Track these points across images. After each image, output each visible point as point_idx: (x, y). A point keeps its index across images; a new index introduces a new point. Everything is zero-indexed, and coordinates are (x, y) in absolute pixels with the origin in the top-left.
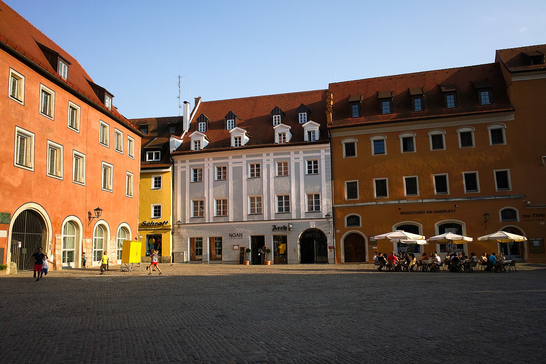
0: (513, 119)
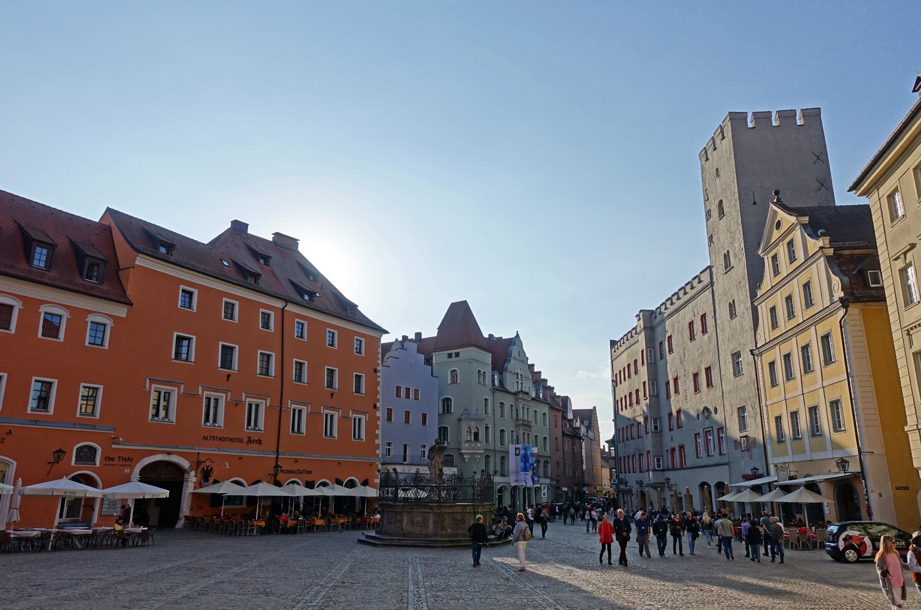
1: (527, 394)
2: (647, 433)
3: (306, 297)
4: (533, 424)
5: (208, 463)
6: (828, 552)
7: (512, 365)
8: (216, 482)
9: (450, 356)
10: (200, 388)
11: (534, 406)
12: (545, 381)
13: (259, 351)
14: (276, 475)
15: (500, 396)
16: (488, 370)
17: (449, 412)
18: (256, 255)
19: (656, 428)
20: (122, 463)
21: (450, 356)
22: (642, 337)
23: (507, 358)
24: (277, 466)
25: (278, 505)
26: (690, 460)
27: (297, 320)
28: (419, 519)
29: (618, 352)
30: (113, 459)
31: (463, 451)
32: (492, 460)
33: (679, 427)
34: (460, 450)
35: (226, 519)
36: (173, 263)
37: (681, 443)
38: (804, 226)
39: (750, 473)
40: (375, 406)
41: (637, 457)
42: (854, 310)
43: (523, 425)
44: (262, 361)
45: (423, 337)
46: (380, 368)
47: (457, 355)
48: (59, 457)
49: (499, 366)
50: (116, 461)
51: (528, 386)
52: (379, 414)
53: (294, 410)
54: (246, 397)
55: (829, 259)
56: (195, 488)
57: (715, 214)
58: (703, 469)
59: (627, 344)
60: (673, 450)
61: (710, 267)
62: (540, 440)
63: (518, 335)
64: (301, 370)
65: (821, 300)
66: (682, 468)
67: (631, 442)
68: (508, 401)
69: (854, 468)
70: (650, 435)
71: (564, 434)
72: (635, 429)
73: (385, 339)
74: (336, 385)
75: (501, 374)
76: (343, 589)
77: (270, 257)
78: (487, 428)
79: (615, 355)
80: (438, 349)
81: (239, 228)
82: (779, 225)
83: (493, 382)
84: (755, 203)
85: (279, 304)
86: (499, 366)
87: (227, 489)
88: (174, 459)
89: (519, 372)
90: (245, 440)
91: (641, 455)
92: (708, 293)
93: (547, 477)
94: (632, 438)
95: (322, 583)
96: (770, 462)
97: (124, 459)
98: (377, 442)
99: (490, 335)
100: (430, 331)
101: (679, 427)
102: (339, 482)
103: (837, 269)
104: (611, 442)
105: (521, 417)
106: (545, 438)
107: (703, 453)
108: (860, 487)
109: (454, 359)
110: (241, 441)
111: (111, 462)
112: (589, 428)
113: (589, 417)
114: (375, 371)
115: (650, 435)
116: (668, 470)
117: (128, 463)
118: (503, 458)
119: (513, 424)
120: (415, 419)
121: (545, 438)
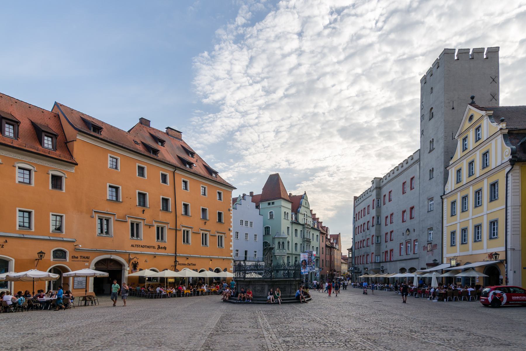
0: (73, 171)
1: (309, 225)
2: (372, 244)
3: (188, 166)
4: (311, 240)
5: (135, 259)
6: (482, 302)
7: (302, 210)
8: (141, 270)
9: (269, 204)
11: (312, 232)
12: (318, 219)
14: (176, 266)
15: (295, 227)
16: (290, 212)
17: (268, 234)
18: (156, 139)
19: (378, 241)
20: (82, 260)
21: (269, 204)
22: (374, 193)
23: (299, 205)
24: (176, 261)
25: (179, 282)
26: (394, 258)
28: (259, 288)
29: (359, 202)
30: (77, 258)
32: (291, 258)
33: (391, 240)
35: (146, 290)
36: (101, 139)
37: (391, 248)
38: (490, 117)
39: (432, 262)
40: (229, 230)
41: (366, 256)
42: (517, 167)
43: (307, 241)
45: (254, 194)
46: (231, 208)
47: (273, 203)
48: (41, 256)
49: (295, 210)
50: (79, 259)
51: (310, 221)
52: (231, 234)
55: (504, 136)
56: (129, 273)
57: (427, 117)
59: (362, 199)
60: (386, 252)
61: (419, 150)
63: (305, 193)
65: (494, 161)
66: (391, 261)
67: (363, 249)
68: (300, 228)
69: (502, 257)
70: (374, 245)
71: (326, 246)
72: (365, 243)
73: (235, 194)
75: (296, 214)
76: (218, 337)
77: (165, 141)
78: (288, 242)
79: (356, 204)
80: (262, 200)
81: (144, 122)
82: (471, 118)
83: (292, 218)
84: (453, 108)
85: (173, 170)
86: (295, 210)
87: (147, 273)
88: (114, 257)
90: (157, 247)
91: (367, 255)
92: (417, 166)
94: (363, 247)
95: (203, 331)
96: (444, 256)
97: (84, 258)
98: (231, 249)
99: (290, 194)
100: (258, 191)
101: (391, 240)
102: (211, 270)
103: (508, 142)
104: (350, 250)
107: (403, 252)
108: (502, 269)
109: (271, 206)
110: (154, 247)
111: (76, 259)
112: (336, 243)
113: (337, 238)
114: (229, 210)
115: (374, 245)
116: (383, 262)
117: (86, 260)
118: (296, 258)
119: (301, 240)
120: (251, 237)
121: (317, 248)
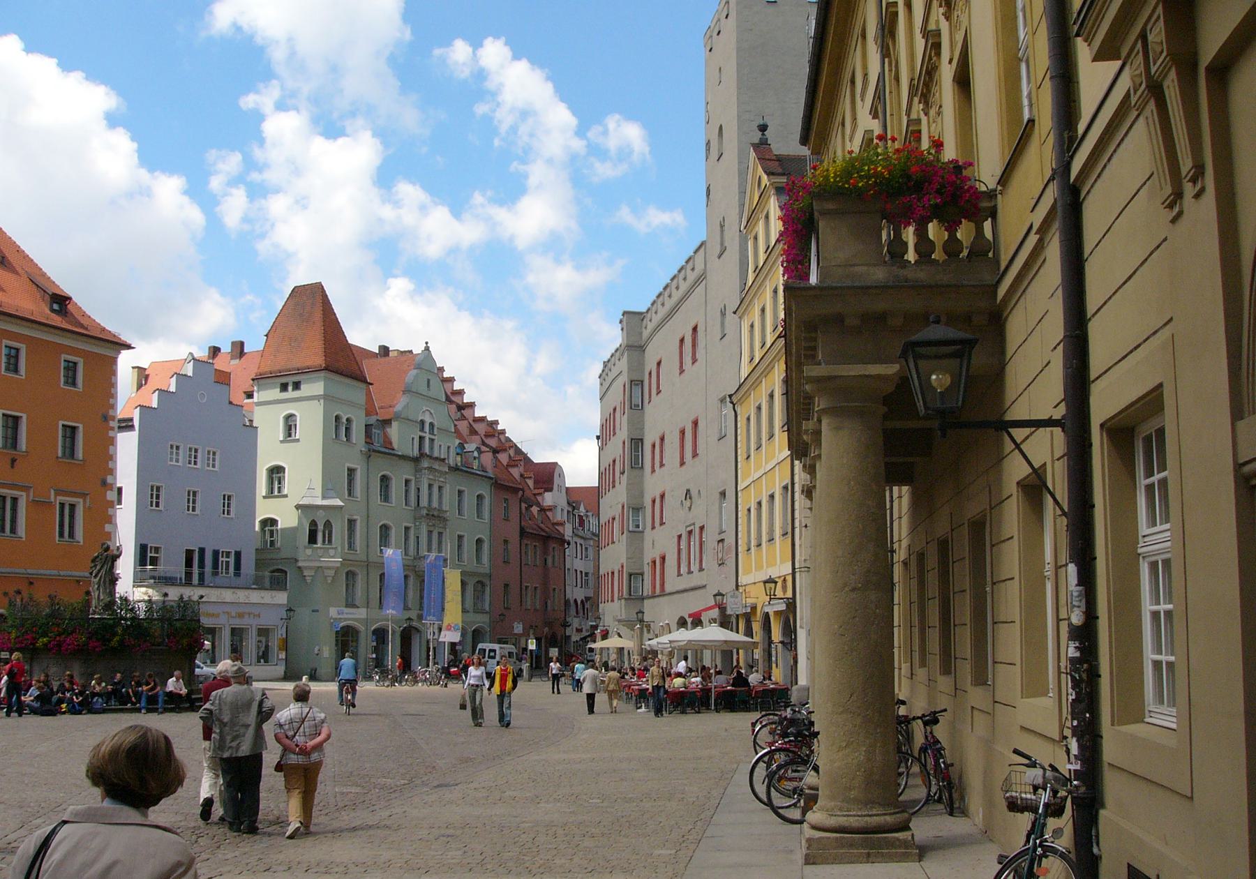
10: (52, 492)
13: (61, 423)
15: (382, 467)
27: (5, 342)
31: (300, 564)
34: (296, 561)
44: (64, 437)
53: (62, 505)
54: (56, 495)
58: (691, 593)
62: (469, 547)
64: (73, 438)
68: (399, 475)
71: (523, 533)
74: (23, 444)
89: (428, 420)
93: (483, 612)
105: (424, 502)
106: (479, 541)
121: (479, 542)
